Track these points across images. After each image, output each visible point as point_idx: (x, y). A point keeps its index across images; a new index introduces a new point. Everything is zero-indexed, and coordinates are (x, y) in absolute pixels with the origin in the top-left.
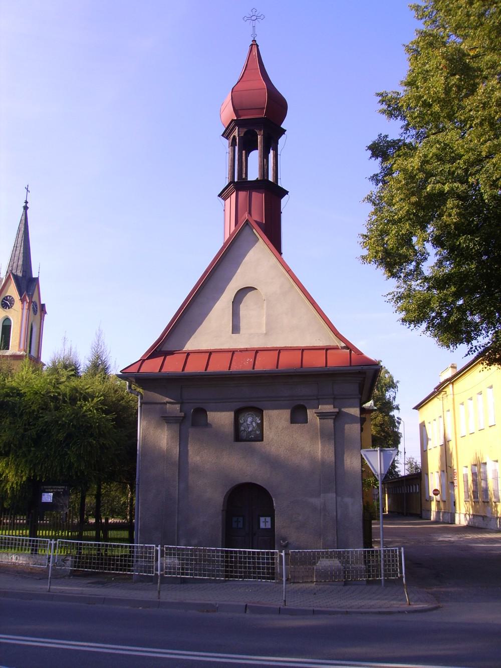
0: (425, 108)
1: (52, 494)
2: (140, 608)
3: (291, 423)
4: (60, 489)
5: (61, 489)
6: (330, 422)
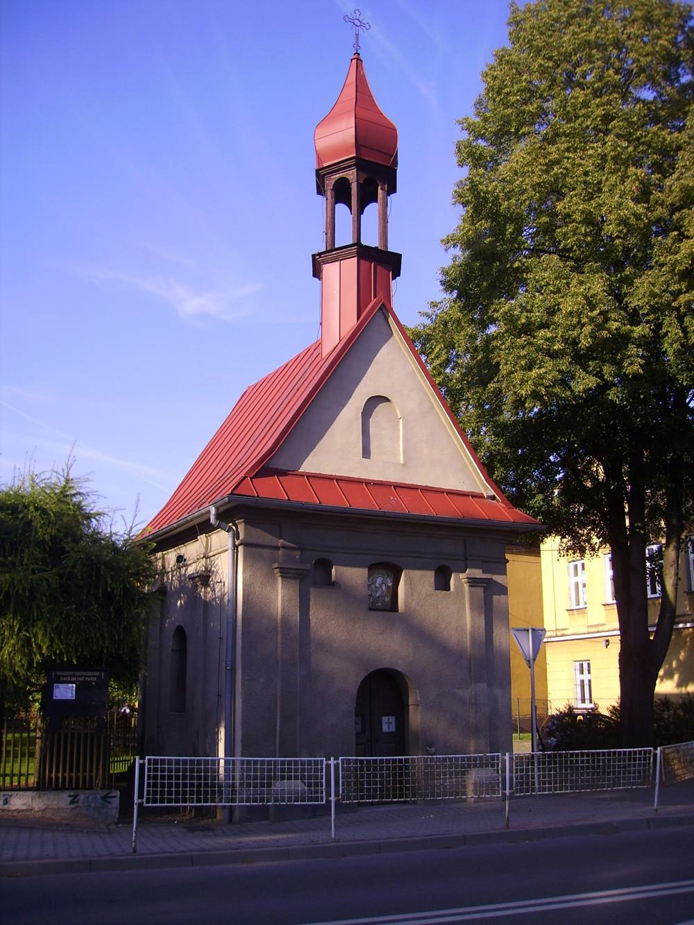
0: (623, 251)
1: (74, 685)
2: (527, 842)
3: (436, 589)
4: (92, 677)
5: (94, 676)
6: (480, 591)
